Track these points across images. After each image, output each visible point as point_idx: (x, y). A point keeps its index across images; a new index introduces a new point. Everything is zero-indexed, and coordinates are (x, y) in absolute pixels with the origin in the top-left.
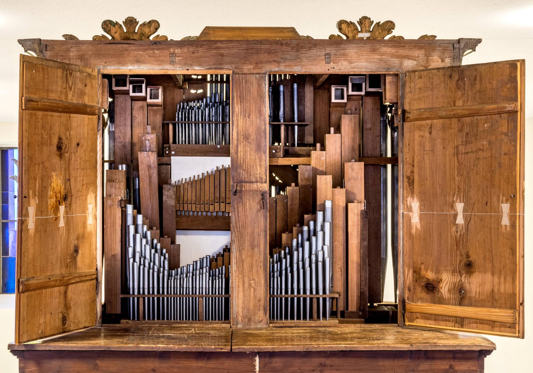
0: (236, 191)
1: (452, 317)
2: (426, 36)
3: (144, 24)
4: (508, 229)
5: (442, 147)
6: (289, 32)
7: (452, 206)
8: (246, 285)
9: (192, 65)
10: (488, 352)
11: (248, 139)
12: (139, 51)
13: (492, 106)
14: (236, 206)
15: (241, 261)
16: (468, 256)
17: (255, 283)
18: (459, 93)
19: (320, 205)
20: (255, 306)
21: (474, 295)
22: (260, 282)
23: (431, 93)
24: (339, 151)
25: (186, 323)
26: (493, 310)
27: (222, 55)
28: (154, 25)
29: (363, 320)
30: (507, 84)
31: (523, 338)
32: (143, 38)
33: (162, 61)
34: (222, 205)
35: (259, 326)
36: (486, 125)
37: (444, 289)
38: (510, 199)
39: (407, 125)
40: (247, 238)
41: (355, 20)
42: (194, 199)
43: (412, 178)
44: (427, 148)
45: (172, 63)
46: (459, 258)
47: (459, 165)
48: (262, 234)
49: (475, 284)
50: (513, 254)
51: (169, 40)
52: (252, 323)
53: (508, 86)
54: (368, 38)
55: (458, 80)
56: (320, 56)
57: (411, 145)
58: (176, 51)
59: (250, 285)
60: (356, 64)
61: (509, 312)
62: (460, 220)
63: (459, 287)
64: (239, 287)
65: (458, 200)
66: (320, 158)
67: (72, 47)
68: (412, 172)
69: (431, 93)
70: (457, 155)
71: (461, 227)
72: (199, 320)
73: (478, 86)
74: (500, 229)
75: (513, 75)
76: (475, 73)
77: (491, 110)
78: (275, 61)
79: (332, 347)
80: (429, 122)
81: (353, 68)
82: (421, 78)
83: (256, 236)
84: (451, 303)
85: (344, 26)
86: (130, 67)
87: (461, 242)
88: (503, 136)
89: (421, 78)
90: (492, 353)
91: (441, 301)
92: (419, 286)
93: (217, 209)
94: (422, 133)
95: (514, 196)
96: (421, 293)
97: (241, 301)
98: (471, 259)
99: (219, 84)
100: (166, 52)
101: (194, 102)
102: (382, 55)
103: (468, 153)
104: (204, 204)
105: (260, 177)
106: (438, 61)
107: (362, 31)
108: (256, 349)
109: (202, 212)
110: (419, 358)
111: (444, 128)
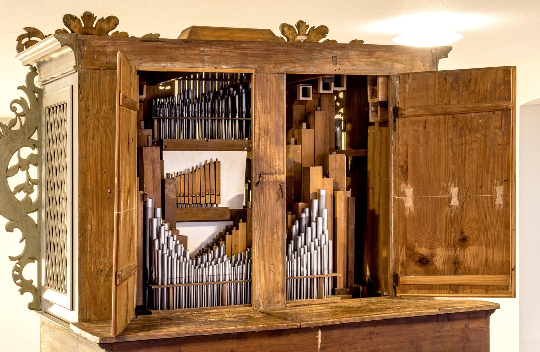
0: (258, 183)
1: (447, 285)
2: (336, 41)
3: (102, 20)
4: (502, 207)
5: (436, 140)
6: (267, 34)
7: (447, 191)
8: (267, 270)
9: (219, 64)
10: (492, 311)
11: (268, 133)
12: (172, 49)
13: (487, 105)
14: (257, 197)
15: (262, 248)
16: (462, 232)
17: (274, 267)
18: (454, 93)
19: (313, 193)
20: (274, 288)
21: (469, 265)
22: (278, 266)
23: (425, 93)
24: (312, 144)
25: (212, 309)
26: (488, 276)
27: (246, 55)
28: (113, 21)
29: (351, 295)
30: (501, 86)
31: (515, 297)
32: (102, 33)
33: (194, 59)
34: (213, 197)
35: (278, 306)
36: (480, 121)
37: (438, 262)
38: (504, 183)
39: (399, 121)
40: (268, 226)
41: (294, 24)
42: (186, 192)
43: (406, 167)
44: (421, 141)
45: (202, 61)
46: (453, 235)
47: (454, 155)
48: (280, 221)
49: (470, 255)
50: (506, 228)
51: (130, 36)
52: (272, 304)
53: (502, 88)
54: (305, 41)
55: (453, 82)
56: (328, 58)
57: (404, 138)
58: (206, 50)
59: (270, 269)
60: (357, 66)
61: (504, 276)
62: (455, 202)
63: (454, 259)
64: (260, 272)
65: (453, 185)
66: (296, 151)
67: (108, 43)
68: (406, 162)
69: (425, 93)
70: (452, 147)
71: (455, 208)
72: (222, 305)
73: (472, 88)
74: (494, 208)
75: (506, 79)
76: (469, 77)
77: (487, 108)
78: (291, 62)
79: (380, 317)
80: (423, 118)
81: (355, 70)
82: (415, 79)
83: (275, 224)
84: (446, 273)
85: (286, 29)
86: (164, 65)
87: (456, 221)
88: (497, 130)
89: (415, 79)
90: (495, 312)
91: (435, 272)
92: (413, 261)
93: (208, 201)
94: (416, 128)
95: (508, 181)
96: (413, 267)
97: (262, 284)
98: (465, 234)
99: (204, 81)
100: (196, 51)
101: (169, 99)
102: (377, 58)
103: (462, 145)
104: (188, 196)
105: (279, 169)
106: (420, 65)
107: (299, 34)
108: (321, 323)
109: (212, 204)
110: (443, 321)
111: (438, 123)
